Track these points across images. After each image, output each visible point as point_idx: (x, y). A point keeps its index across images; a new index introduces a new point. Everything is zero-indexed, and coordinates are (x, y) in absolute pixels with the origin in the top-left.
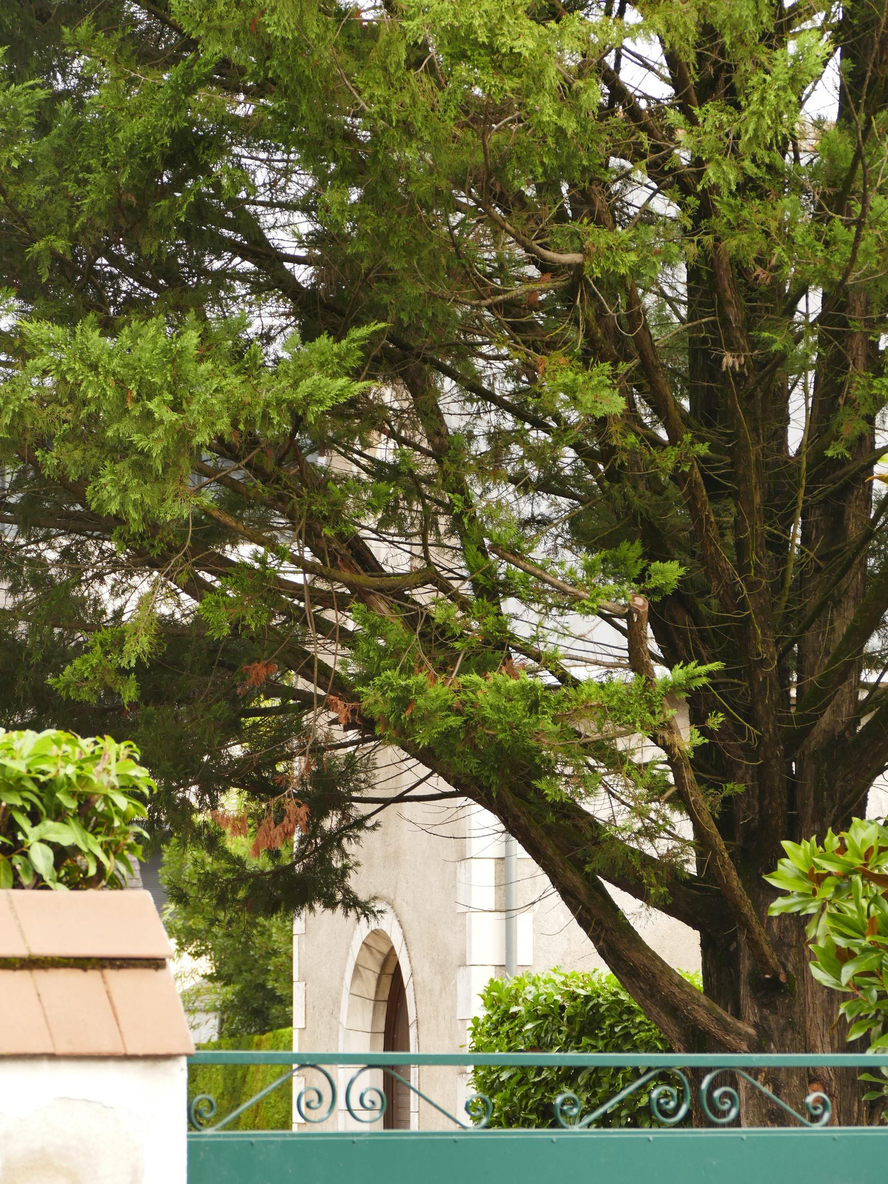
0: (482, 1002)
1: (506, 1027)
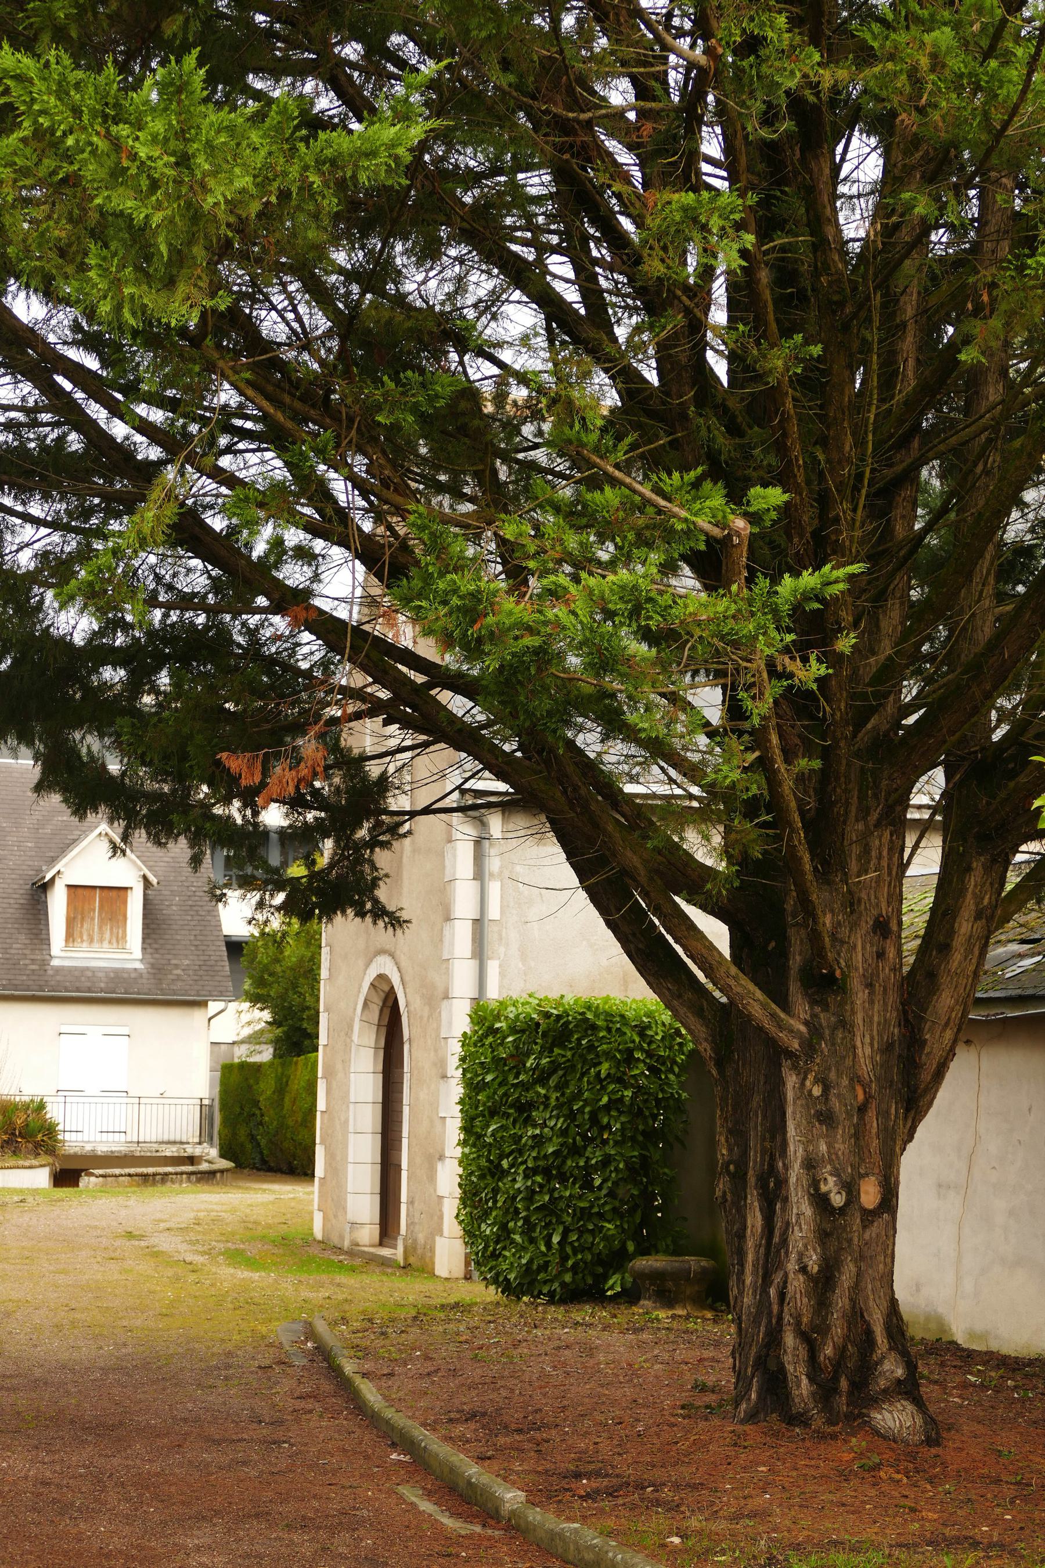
0: (468, 1019)
1: (490, 1039)
